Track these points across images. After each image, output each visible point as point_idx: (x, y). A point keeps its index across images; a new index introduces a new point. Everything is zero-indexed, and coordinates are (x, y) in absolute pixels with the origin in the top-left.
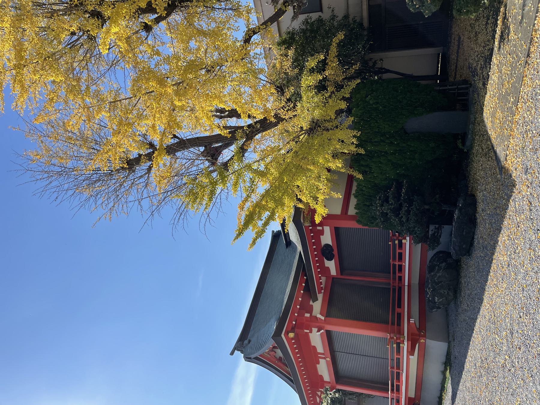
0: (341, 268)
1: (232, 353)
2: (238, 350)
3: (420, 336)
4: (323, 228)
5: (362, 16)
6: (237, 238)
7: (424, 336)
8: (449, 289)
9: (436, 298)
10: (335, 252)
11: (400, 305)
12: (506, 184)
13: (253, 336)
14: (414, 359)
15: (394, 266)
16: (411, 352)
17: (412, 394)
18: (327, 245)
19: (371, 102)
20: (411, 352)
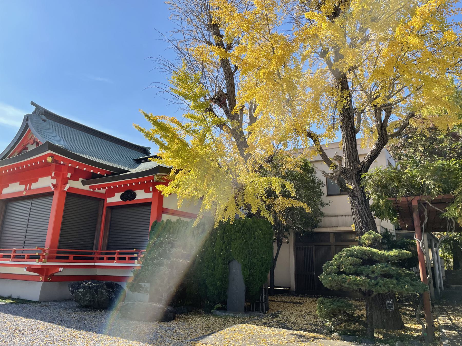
0: (113, 207)
1: (33, 103)
2: (36, 110)
3: (46, 276)
5: (322, 227)
7: (46, 280)
8: (90, 301)
9: (82, 290)
10: (128, 202)
11: (76, 259)
14: (23, 271)
15: (114, 254)
16: (30, 269)
18: (135, 195)
19: (256, 233)
20: (30, 269)
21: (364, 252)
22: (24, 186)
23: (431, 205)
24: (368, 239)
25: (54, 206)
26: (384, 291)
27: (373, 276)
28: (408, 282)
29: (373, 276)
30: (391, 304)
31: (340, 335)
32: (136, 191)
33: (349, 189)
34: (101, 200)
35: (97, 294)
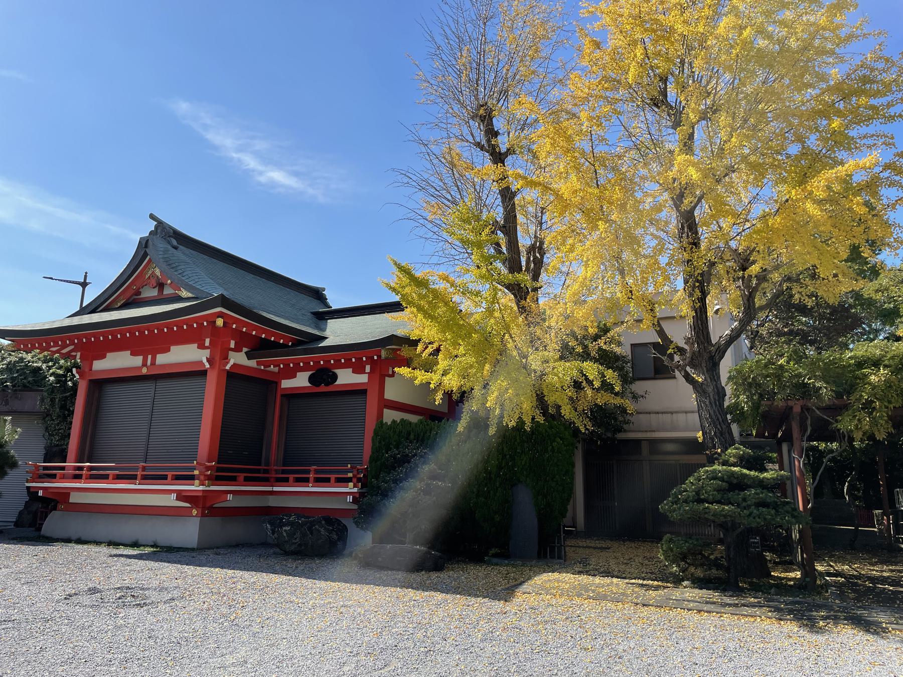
1: (152, 217)
2: (156, 227)
3: (204, 508)
4: (207, 348)
5: (629, 431)
6: (395, 264)
7: (203, 515)
8: (300, 545)
9: (288, 528)
10: (323, 388)
11: (248, 480)
12: (506, 593)
13: (182, 254)
14: (171, 501)
15: (308, 472)
16: (181, 496)
17: (74, 498)
18: (335, 377)
19: (555, 444)
20: (181, 496)
21: (733, 474)
22: (140, 358)
23: (818, 412)
24: (734, 456)
25: (211, 392)
26: (758, 523)
27: (744, 504)
28: (788, 512)
29: (744, 504)
30: (757, 543)
31: (693, 582)
32: (338, 371)
33: (697, 381)
34: (268, 384)
35: (312, 533)
